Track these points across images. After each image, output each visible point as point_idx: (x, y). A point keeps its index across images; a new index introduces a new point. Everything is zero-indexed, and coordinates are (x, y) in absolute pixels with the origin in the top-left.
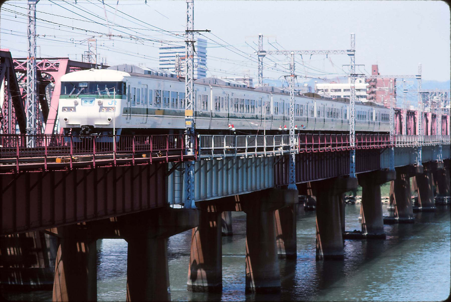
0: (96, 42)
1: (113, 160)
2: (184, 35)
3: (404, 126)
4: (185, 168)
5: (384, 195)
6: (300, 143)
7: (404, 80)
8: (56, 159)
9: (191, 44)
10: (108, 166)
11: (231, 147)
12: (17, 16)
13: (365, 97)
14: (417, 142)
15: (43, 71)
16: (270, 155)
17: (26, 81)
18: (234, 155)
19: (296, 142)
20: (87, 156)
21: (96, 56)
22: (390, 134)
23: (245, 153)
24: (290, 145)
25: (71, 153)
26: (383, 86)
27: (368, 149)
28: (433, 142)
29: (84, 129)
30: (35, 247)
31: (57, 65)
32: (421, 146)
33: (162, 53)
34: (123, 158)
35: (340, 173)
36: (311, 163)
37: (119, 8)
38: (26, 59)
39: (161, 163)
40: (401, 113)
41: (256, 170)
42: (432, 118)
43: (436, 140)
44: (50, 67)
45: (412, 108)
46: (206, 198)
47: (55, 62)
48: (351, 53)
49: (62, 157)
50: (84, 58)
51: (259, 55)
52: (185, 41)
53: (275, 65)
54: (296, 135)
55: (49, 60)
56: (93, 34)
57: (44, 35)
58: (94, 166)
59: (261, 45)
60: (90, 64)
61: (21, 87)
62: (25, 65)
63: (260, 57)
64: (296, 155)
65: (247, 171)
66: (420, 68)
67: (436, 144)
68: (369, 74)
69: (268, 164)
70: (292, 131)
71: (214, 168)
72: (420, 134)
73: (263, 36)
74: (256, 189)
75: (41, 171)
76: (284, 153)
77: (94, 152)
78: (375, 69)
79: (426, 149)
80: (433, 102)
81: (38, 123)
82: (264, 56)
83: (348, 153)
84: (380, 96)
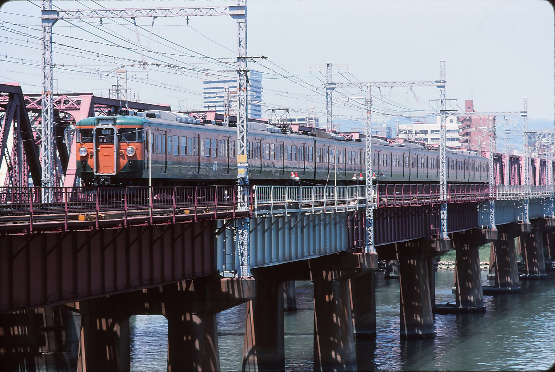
0: (126, 73)
1: (149, 217)
2: (235, 63)
3: (507, 174)
4: (237, 227)
5: (484, 259)
6: (379, 196)
7: (506, 119)
8: (79, 216)
9: (243, 74)
10: (142, 225)
11: (294, 201)
12: (28, 41)
13: (458, 139)
14: (522, 194)
15: (61, 109)
16: (342, 210)
17: (40, 123)
18: (298, 210)
19: (375, 194)
20: (117, 212)
21: (126, 90)
22: (490, 184)
23: (311, 208)
24: (367, 198)
25: (98, 209)
26: (481, 126)
27: (462, 202)
28: (543, 194)
29: (103, 179)
30: (45, 325)
31: (78, 103)
32: (528, 198)
33: (207, 89)
34: (161, 215)
35: (428, 233)
36: (392, 220)
37: (155, 30)
38: (40, 95)
39: (207, 220)
40: (502, 159)
41: (325, 229)
42: (541, 165)
43: (547, 192)
44: (70, 105)
45: (516, 153)
46: (264, 263)
47: (76, 98)
48: (441, 84)
49: (86, 213)
50: (112, 93)
51: (327, 88)
52: (237, 70)
53: (347, 100)
54: (374, 185)
55: (69, 97)
56: (124, 63)
57: (62, 64)
58: (125, 224)
59: (329, 76)
60: (119, 100)
61: (35, 130)
62: (39, 103)
63: (328, 91)
64: (374, 210)
65: (314, 231)
66: (525, 102)
67: (547, 197)
68: (462, 111)
69: (340, 222)
70: (368, 181)
71: (273, 226)
72: (526, 184)
73: (331, 65)
74: (326, 252)
75: (60, 230)
76: (359, 208)
77: (126, 208)
78: (470, 105)
79: (534, 203)
80: (541, 145)
81: (55, 175)
82: (334, 89)
83: (438, 206)
84: (476, 138)
